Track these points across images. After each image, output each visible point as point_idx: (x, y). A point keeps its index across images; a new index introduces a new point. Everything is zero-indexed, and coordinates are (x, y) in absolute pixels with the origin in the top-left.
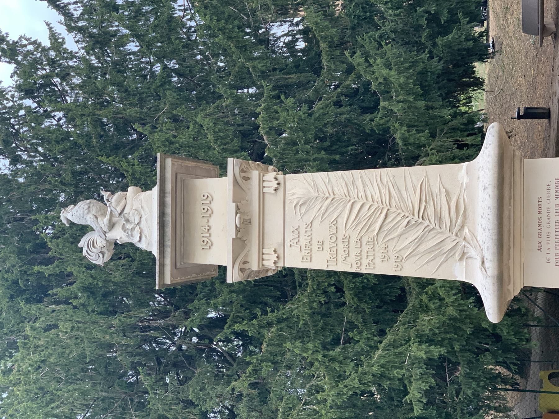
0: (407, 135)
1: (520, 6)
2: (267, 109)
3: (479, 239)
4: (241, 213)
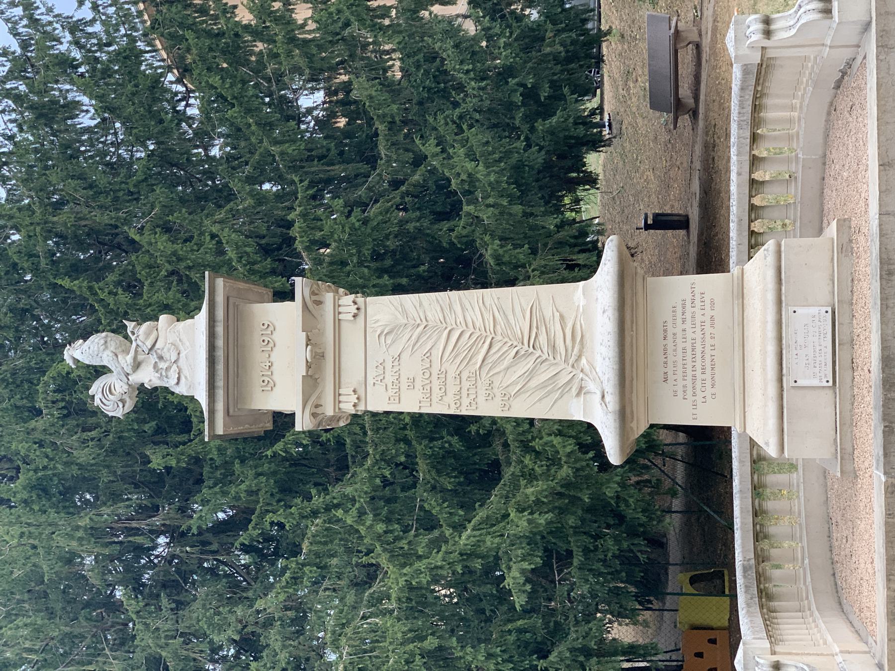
0: (501, 251)
1: (646, 71)
2: (304, 215)
3: (598, 370)
4: (312, 344)
